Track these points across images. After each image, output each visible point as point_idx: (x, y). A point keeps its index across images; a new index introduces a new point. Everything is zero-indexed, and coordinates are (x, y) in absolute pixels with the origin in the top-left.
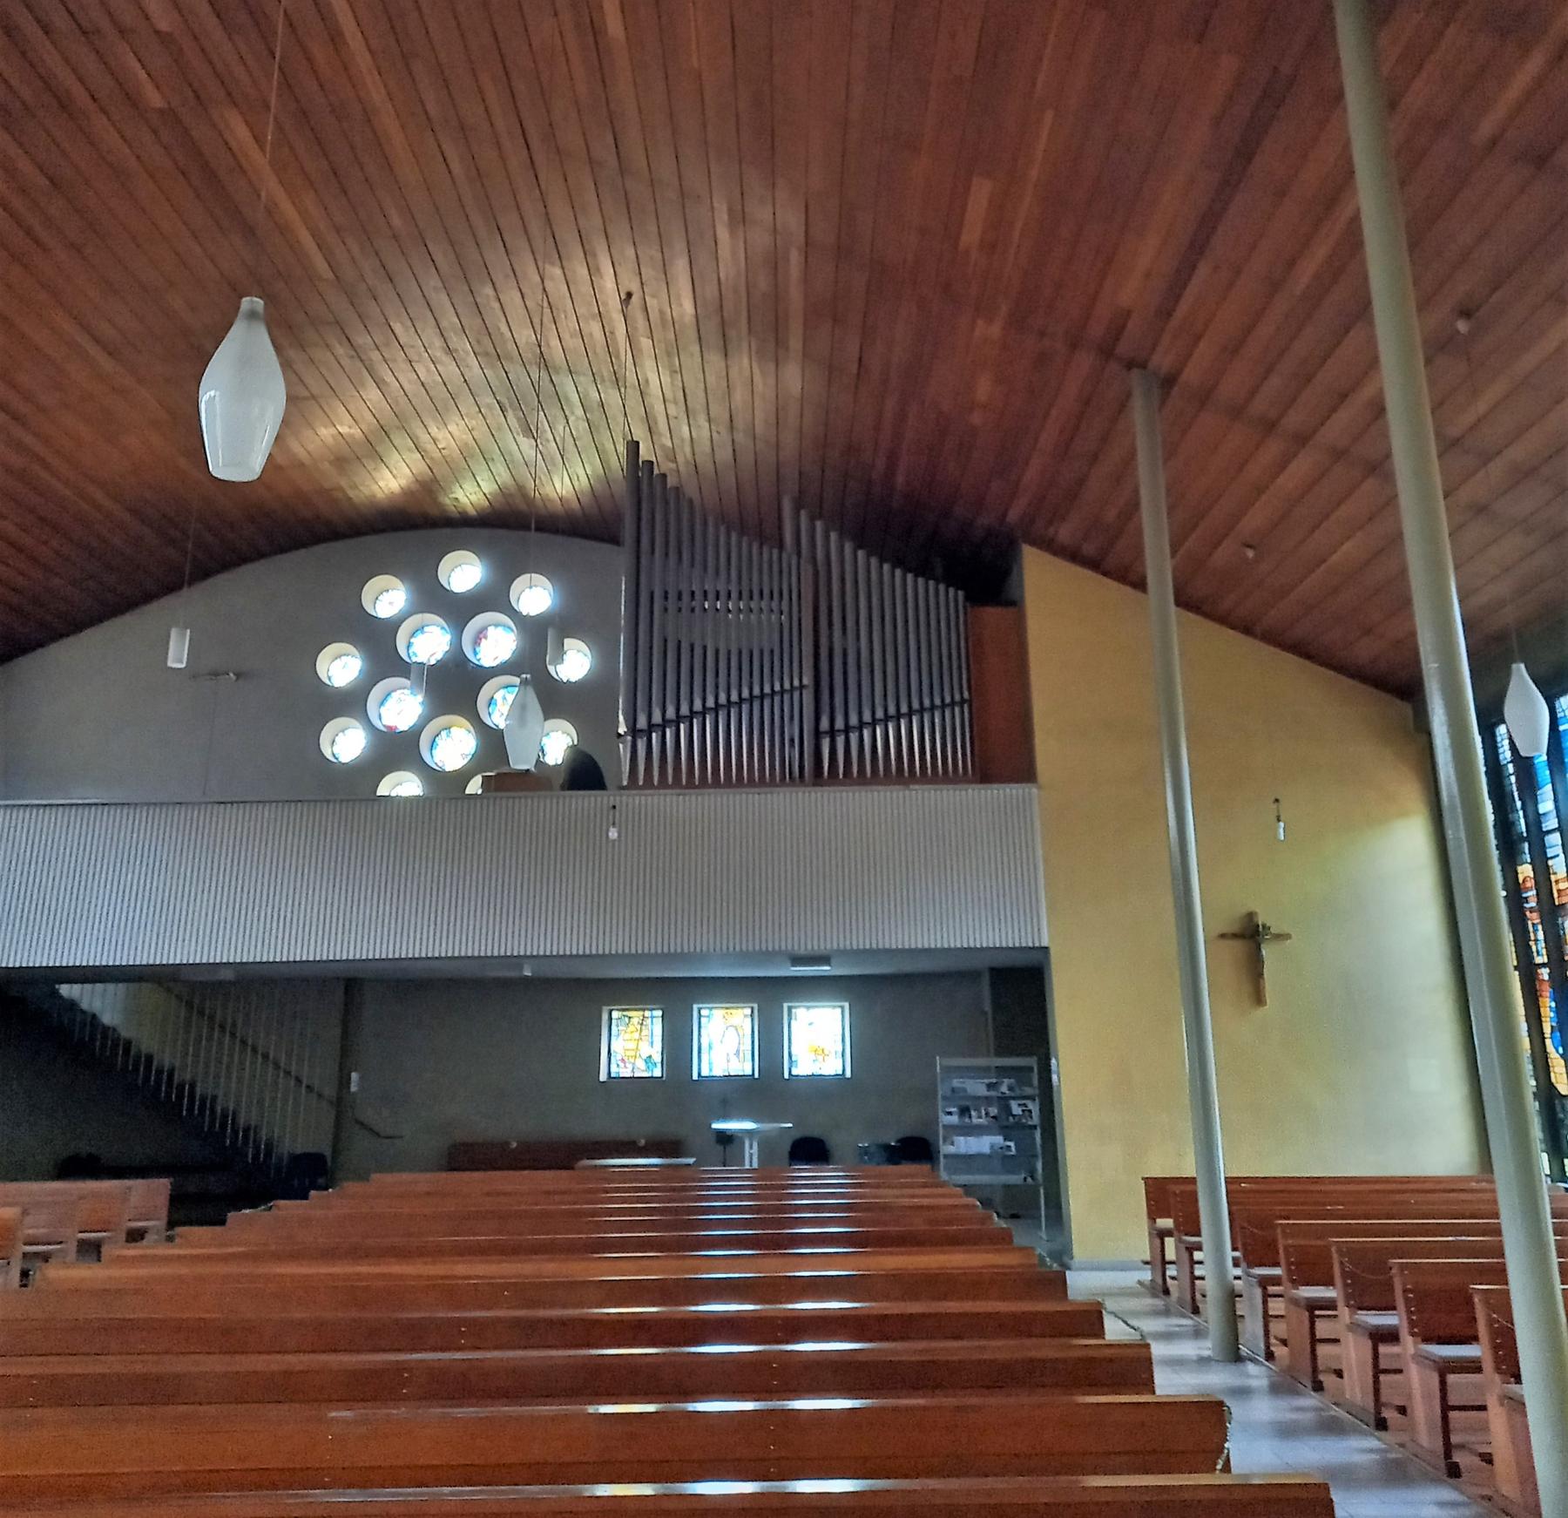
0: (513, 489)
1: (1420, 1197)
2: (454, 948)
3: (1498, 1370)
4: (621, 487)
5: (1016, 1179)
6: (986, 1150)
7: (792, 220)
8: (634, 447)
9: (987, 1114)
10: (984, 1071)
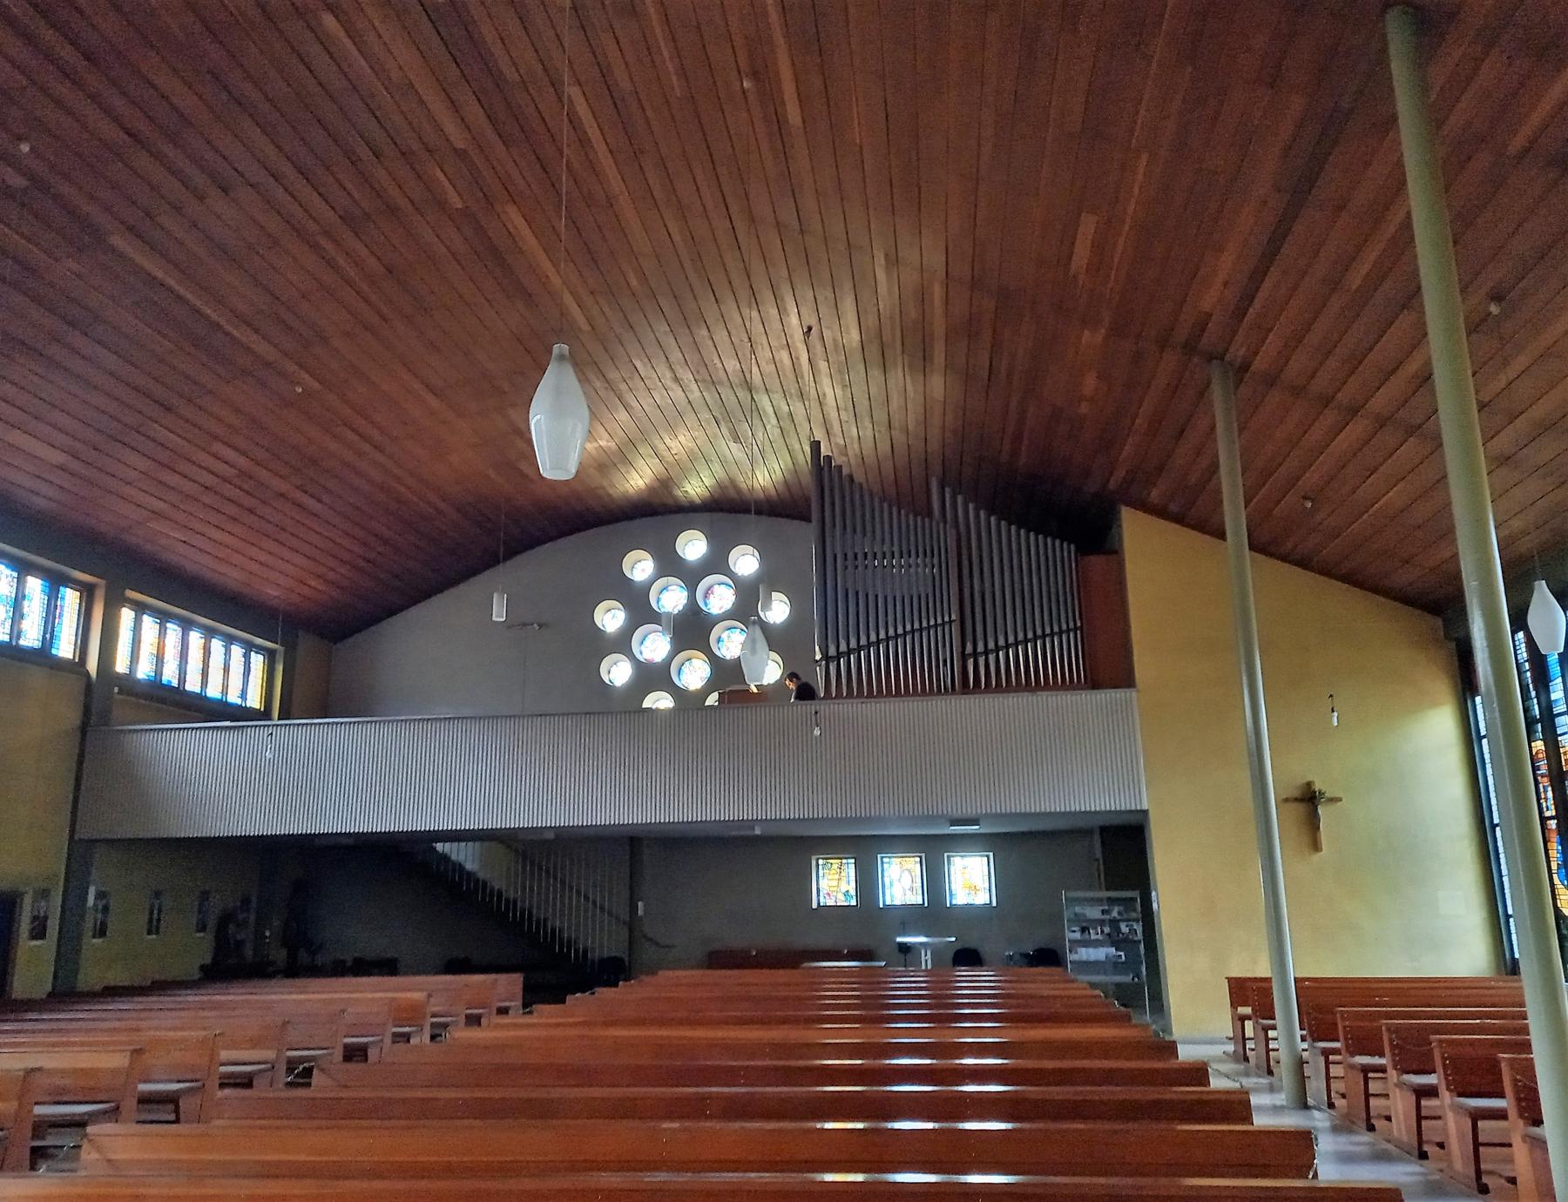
0: (727, 483)
1: (1449, 992)
3: (1521, 1116)
4: (807, 480)
5: (1127, 979)
7: (936, 260)
8: (816, 446)
9: (1102, 932)
10: (1099, 901)
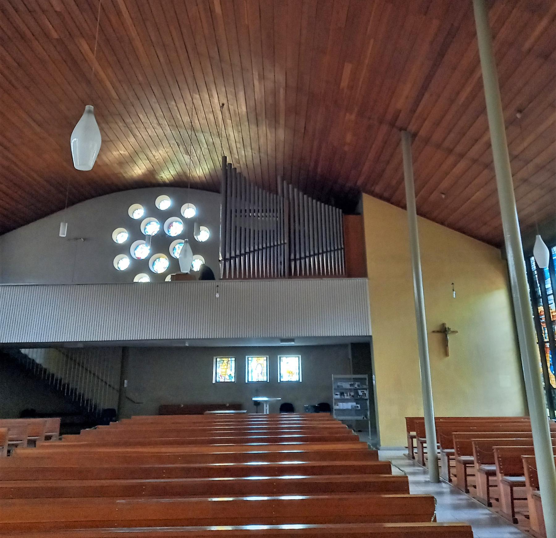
0: (182, 173)
1: (503, 424)
2: (161, 336)
3: (531, 485)
4: (220, 173)
5: (360, 418)
6: (350, 408)
7: (281, 78)
8: (225, 158)
9: (350, 395)
10: (349, 380)
